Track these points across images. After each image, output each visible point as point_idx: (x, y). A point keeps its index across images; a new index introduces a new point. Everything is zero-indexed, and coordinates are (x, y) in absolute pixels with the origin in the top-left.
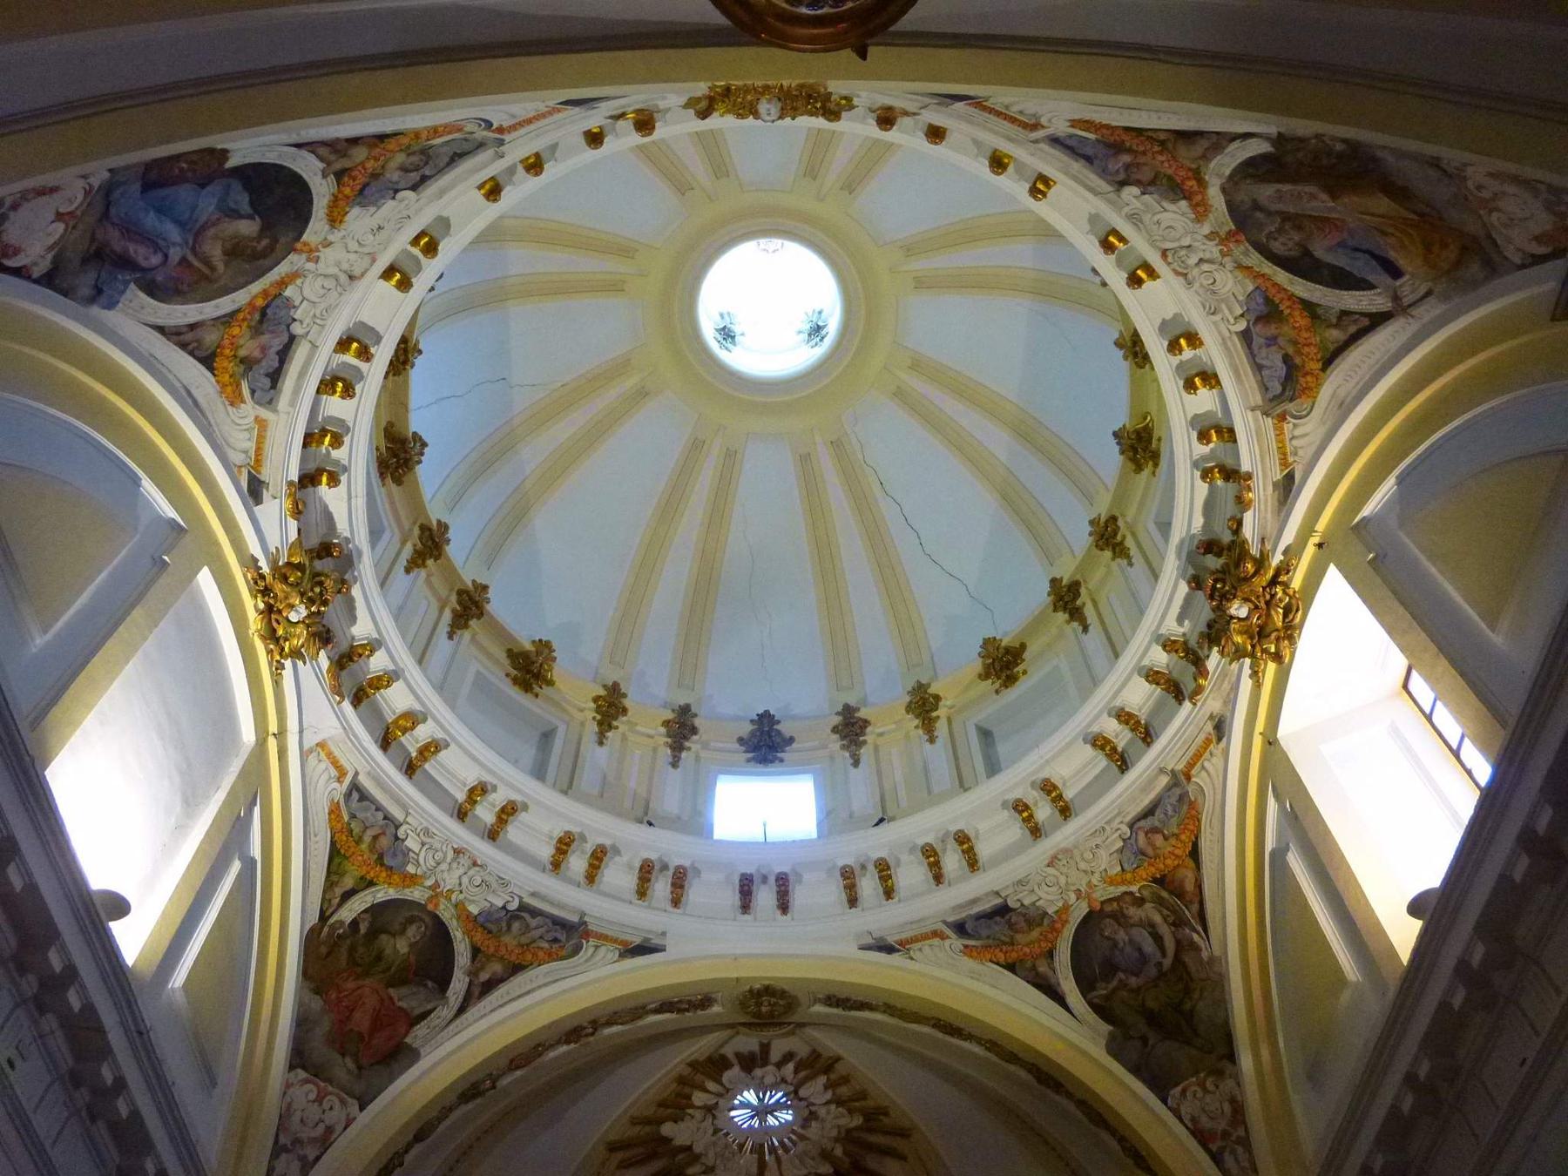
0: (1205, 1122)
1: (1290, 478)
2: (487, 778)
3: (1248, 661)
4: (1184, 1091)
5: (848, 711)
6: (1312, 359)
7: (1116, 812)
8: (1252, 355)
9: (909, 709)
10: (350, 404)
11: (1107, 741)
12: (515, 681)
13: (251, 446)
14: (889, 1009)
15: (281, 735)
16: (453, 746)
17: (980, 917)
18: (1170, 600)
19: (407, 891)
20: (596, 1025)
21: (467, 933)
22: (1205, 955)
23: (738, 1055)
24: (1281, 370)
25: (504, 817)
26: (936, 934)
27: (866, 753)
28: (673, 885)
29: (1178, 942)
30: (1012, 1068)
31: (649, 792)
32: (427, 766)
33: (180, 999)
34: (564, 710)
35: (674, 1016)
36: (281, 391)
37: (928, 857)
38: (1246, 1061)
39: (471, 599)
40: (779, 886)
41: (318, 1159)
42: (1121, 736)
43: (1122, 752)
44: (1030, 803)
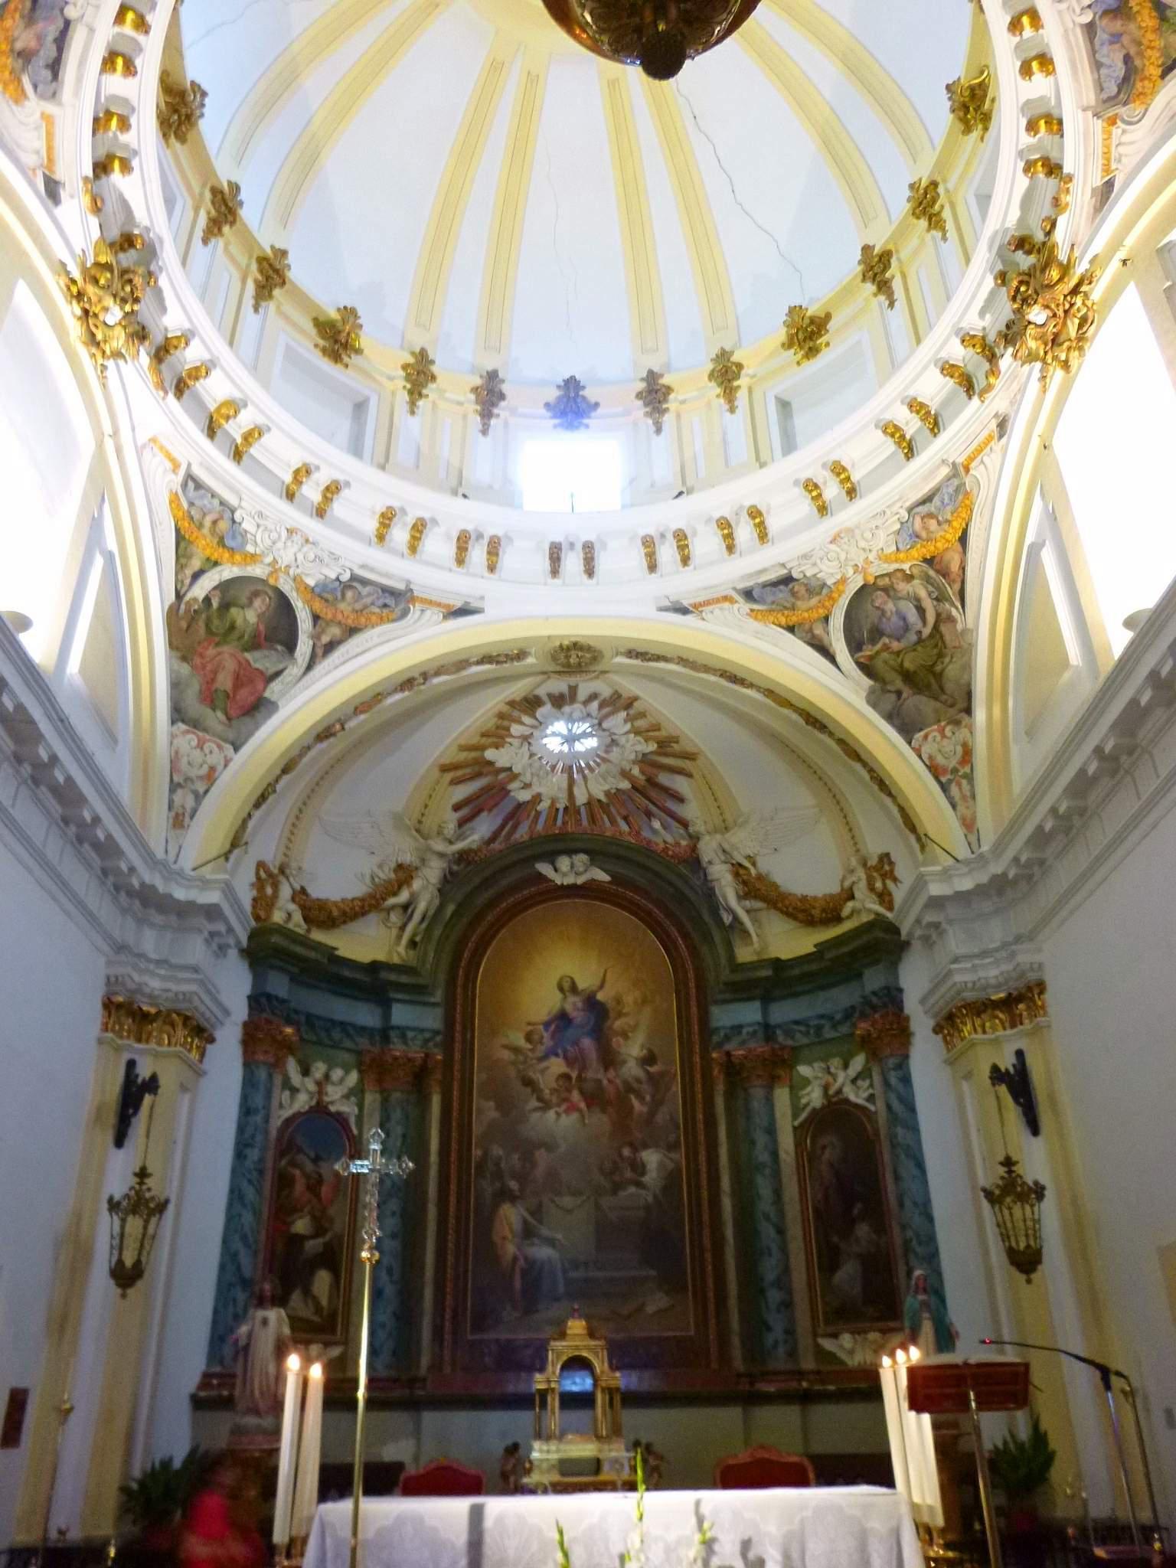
0: (940, 760)
1: (1109, 185)
2: (311, 460)
3: (1038, 365)
4: (926, 737)
5: (652, 377)
6: (1153, 64)
7: (897, 497)
8: (1093, 52)
9: (711, 376)
10: (131, 81)
11: (897, 428)
12: (324, 351)
13: (41, 145)
14: (682, 661)
15: (115, 434)
16: (274, 429)
17: (765, 585)
18: (974, 296)
19: (249, 568)
20: (425, 676)
21: (307, 602)
22: (959, 627)
23: (550, 696)
24: (1120, 70)
25: (329, 495)
26: (726, 598)
27: (668, 419)
28: (489, 553)
29: (938, 615)
30: (786, 711)
31: (462, 462)
32: (252, 451)
33: (78, 681)
34: (374, 380)
35: (494, 666)
36: (63, 82)
37: (723, 529)
38: (980, 714)
39: (271, 265)
40: (586, 554)
41: (206, 792)
42: (912, 425)
43: (910, 440)
44: (819, 481)
